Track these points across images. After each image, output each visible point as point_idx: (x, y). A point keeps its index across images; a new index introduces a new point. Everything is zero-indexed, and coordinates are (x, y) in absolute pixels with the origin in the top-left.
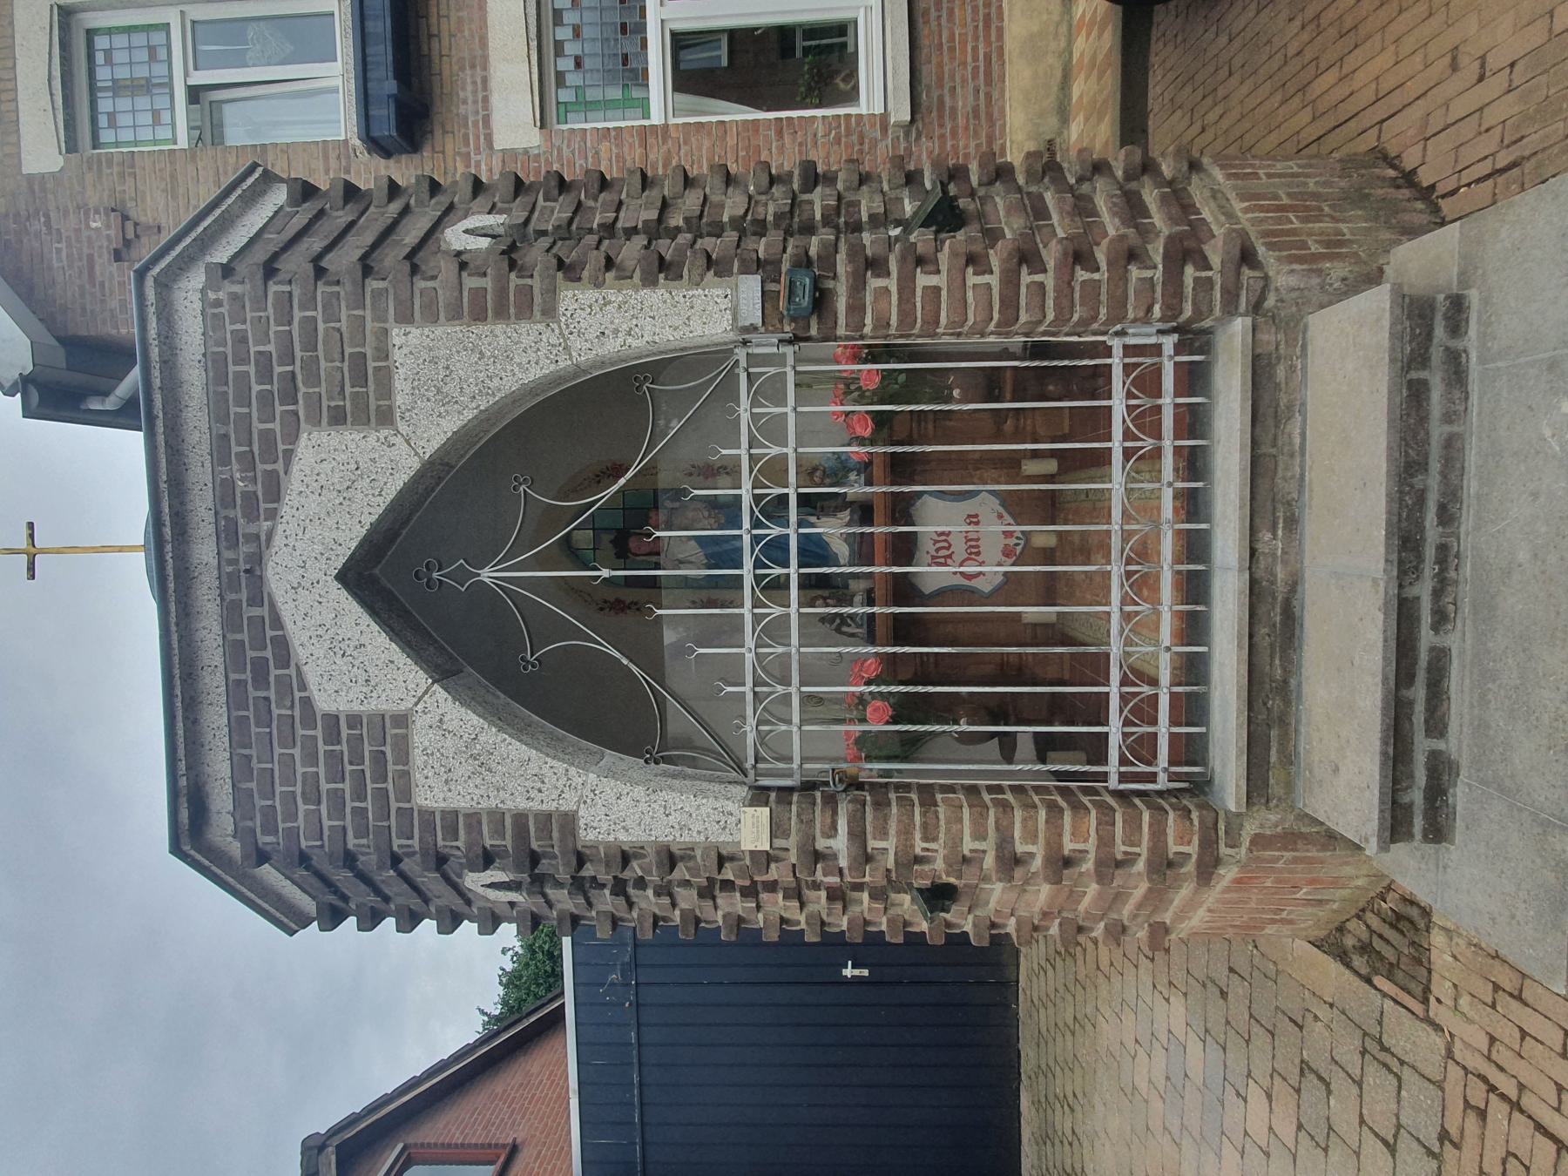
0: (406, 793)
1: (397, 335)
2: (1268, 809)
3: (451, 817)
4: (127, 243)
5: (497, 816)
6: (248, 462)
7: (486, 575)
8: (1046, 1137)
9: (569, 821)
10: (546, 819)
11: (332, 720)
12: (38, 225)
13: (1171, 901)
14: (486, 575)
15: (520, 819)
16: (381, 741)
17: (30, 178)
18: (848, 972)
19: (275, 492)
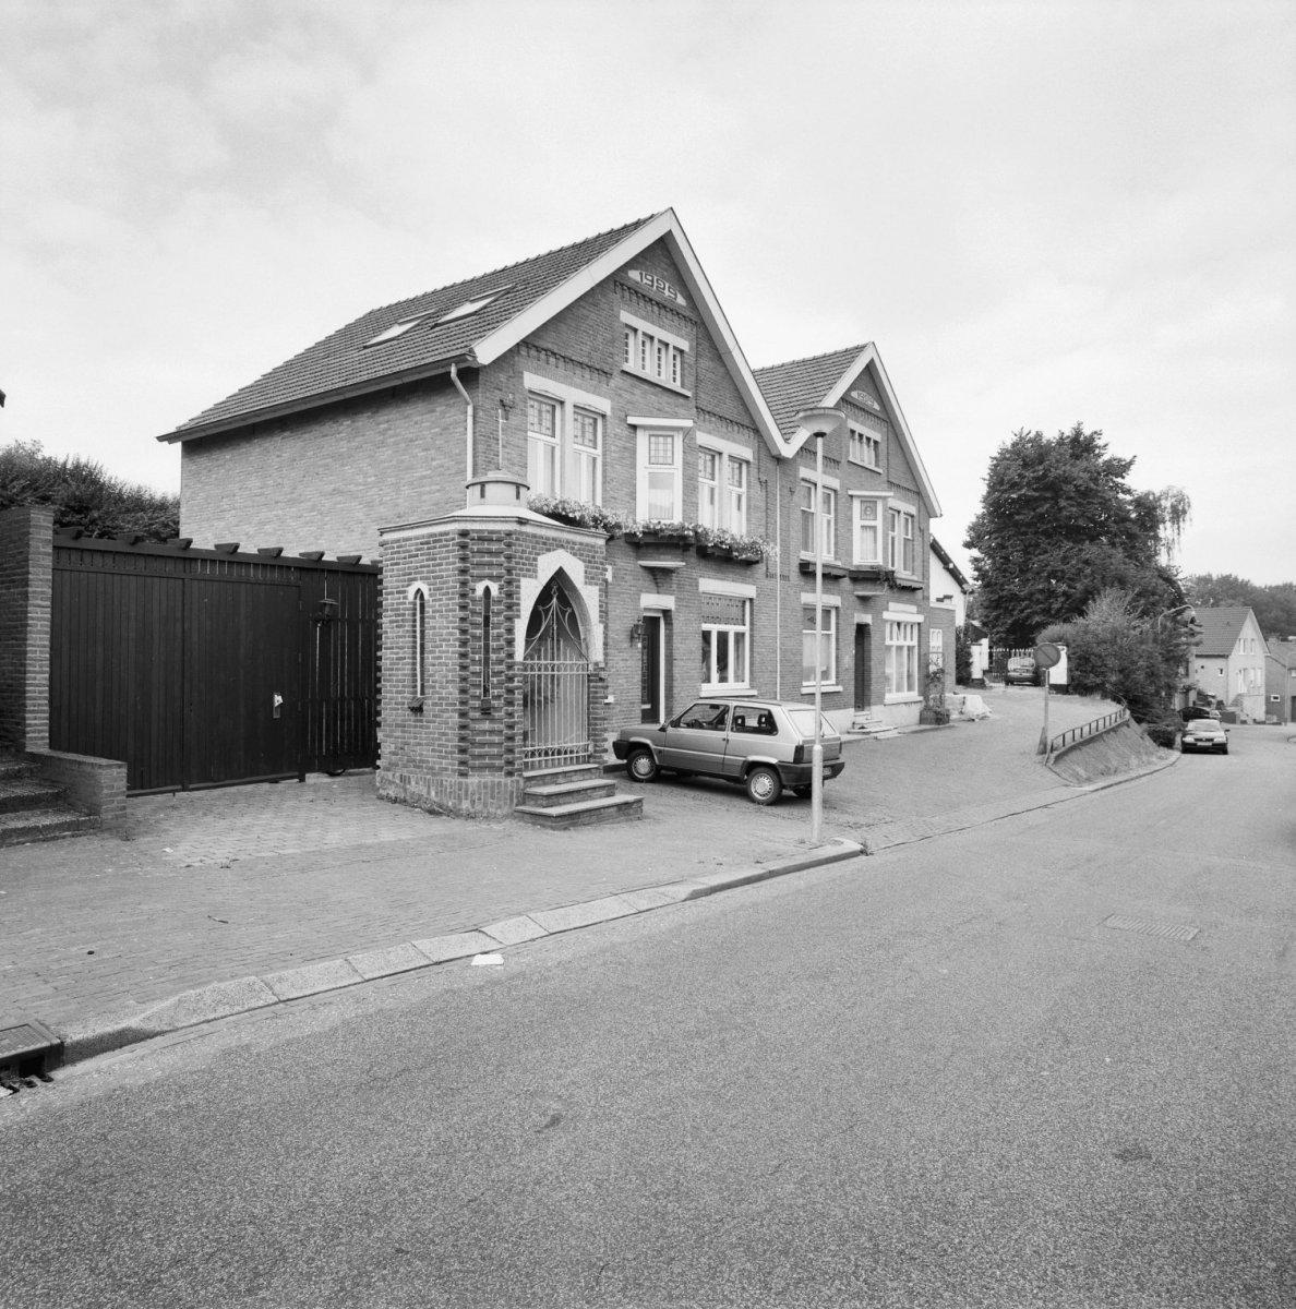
0: (524, 576)
1: (598, 587)
2: (346, 1023)
3: (518, 587)
4: (504, 406)
5: (518, 599)
6: (579, 549)
7: (555, 599)
8: (252, 795)
9: (518, 617)
10: (519, 611)
11: (535, 560)
12: (511, 373)
13: (876, 590)
14: (555, 599)
15: (518, 605)
16: (532, 572)
17: (522, 373)
18: (278, 700)
19: (575, 555)
